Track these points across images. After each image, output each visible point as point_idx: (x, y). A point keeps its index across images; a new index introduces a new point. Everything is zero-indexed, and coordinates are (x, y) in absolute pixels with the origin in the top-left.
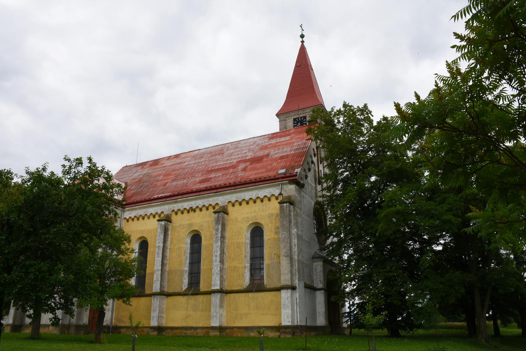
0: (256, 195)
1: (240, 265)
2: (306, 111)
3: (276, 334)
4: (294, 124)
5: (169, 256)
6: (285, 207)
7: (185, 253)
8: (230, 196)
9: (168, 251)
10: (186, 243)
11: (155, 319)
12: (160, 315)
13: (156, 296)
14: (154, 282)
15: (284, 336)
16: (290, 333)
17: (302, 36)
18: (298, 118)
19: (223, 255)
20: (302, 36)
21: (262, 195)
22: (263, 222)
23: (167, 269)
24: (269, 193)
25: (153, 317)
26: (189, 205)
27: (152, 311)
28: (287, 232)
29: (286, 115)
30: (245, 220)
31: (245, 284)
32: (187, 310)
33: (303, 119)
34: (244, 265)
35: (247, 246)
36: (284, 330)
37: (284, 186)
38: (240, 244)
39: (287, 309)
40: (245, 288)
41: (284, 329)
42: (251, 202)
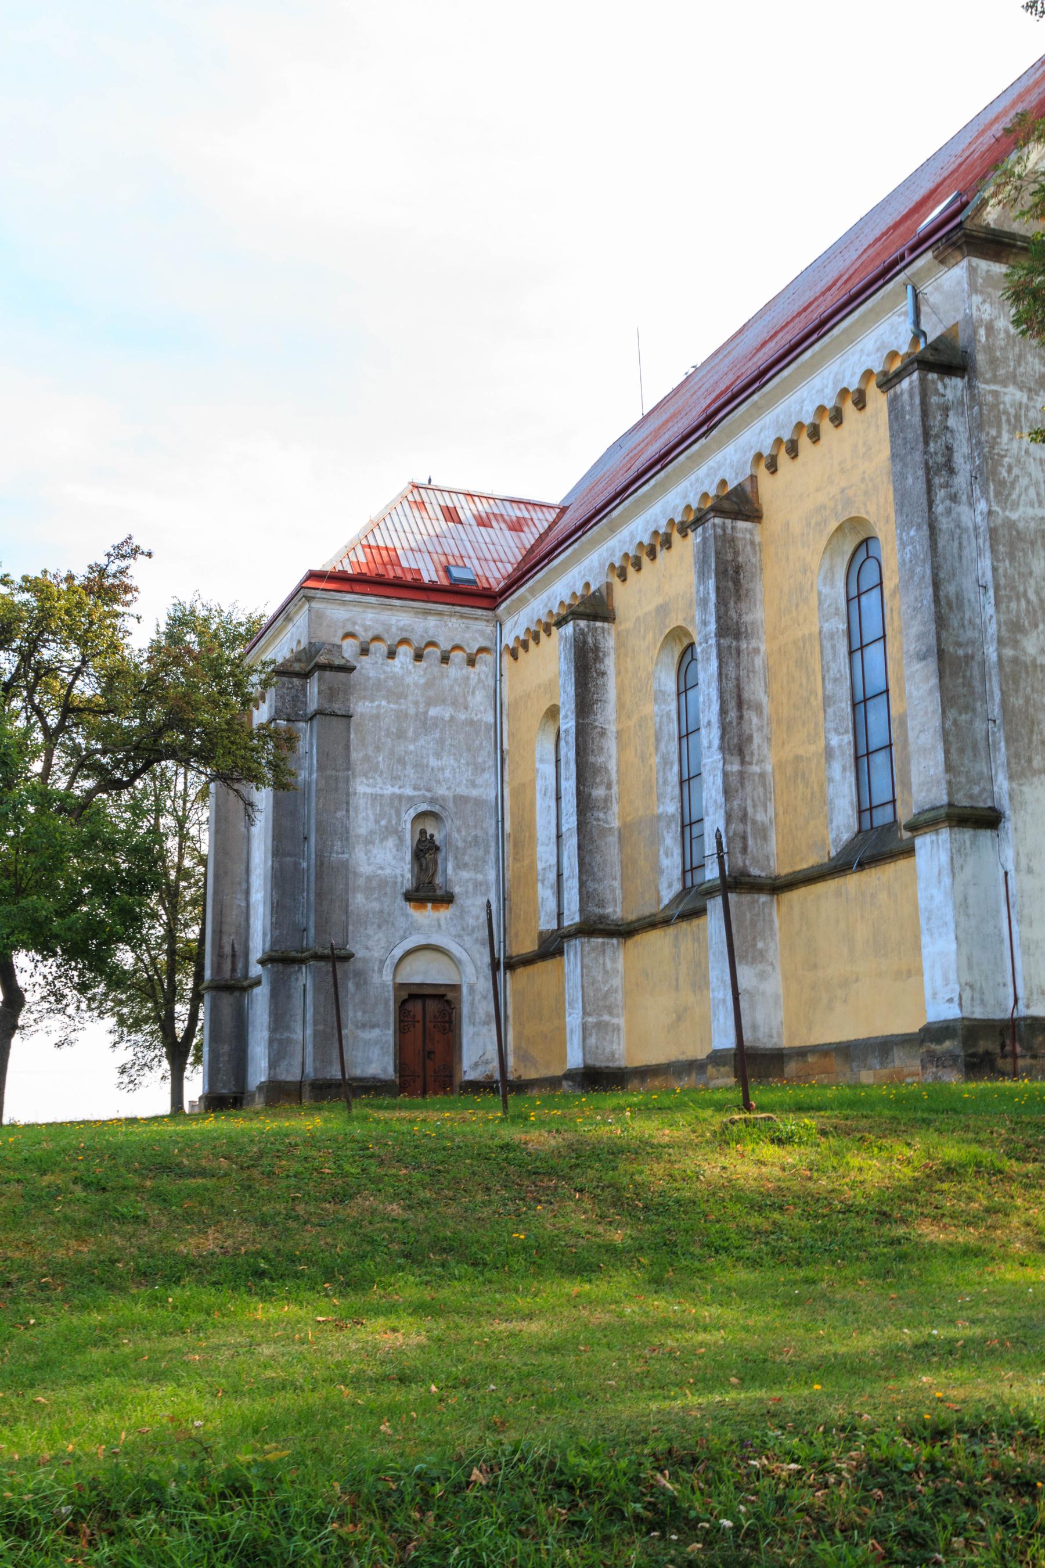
1: (812, 748)
5: (618, 765)
7: (658, 740)
9: (611, 745)
10: (659, 696)
12: (591, 1020)
19: (741, 717)
23: (616, 824)
28: (919, 527)
30: (813, 522)
31: (832, 836)
32: (677, 988)
35: (833, 647)
38: (804, 643)
40: (833, 854)
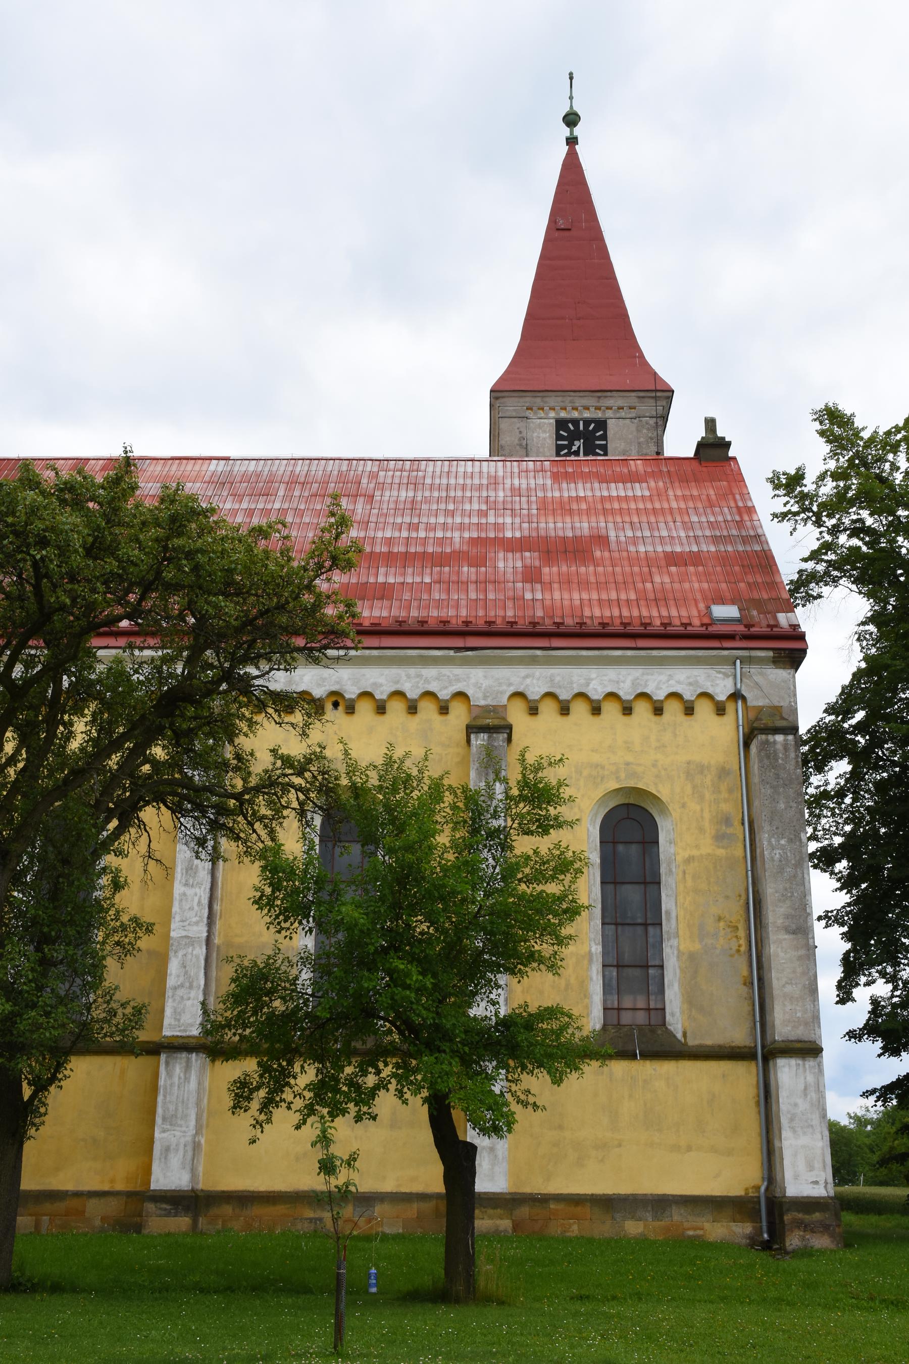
0: (634, 683)
2: (610, 402)
3: (734, 1228)
4: (557, 440)
6: (779, 747)
8: (522, 671)
11: (175, 1160)
13: (184, 1055)
14: (169, 993)
15: (803, 1239)
16: (825, 1228)
17: (571, 119)
18: (575, 422)
20: (571, 119)
21: (658, 688)
22: (663, 791)
24: (690, 684)
25: (167, 1149)
26: (324, 680)
27: (159, 1120)
29: (528, 400)
33: (596, 430)
34: (587, 949)
36: (800, 1216)
37: (754, 670)
39: (804, 1133)
41: (799, 1212)
42: (611, 710)
